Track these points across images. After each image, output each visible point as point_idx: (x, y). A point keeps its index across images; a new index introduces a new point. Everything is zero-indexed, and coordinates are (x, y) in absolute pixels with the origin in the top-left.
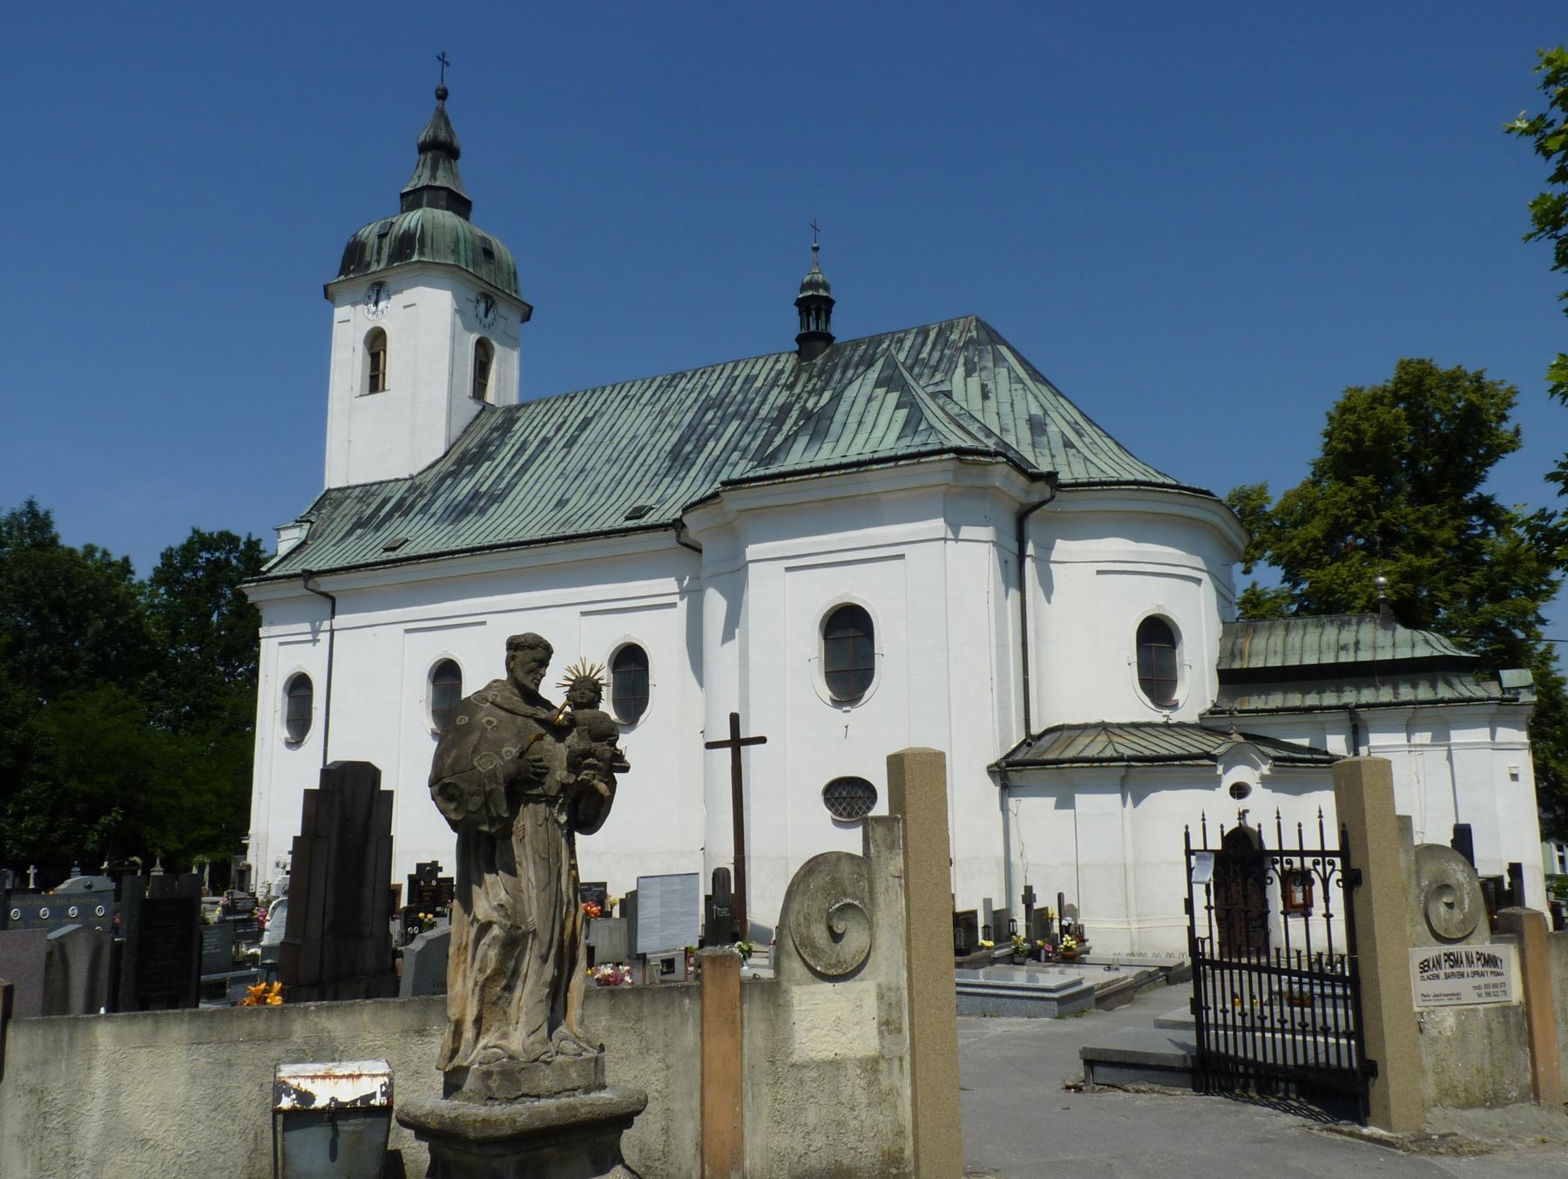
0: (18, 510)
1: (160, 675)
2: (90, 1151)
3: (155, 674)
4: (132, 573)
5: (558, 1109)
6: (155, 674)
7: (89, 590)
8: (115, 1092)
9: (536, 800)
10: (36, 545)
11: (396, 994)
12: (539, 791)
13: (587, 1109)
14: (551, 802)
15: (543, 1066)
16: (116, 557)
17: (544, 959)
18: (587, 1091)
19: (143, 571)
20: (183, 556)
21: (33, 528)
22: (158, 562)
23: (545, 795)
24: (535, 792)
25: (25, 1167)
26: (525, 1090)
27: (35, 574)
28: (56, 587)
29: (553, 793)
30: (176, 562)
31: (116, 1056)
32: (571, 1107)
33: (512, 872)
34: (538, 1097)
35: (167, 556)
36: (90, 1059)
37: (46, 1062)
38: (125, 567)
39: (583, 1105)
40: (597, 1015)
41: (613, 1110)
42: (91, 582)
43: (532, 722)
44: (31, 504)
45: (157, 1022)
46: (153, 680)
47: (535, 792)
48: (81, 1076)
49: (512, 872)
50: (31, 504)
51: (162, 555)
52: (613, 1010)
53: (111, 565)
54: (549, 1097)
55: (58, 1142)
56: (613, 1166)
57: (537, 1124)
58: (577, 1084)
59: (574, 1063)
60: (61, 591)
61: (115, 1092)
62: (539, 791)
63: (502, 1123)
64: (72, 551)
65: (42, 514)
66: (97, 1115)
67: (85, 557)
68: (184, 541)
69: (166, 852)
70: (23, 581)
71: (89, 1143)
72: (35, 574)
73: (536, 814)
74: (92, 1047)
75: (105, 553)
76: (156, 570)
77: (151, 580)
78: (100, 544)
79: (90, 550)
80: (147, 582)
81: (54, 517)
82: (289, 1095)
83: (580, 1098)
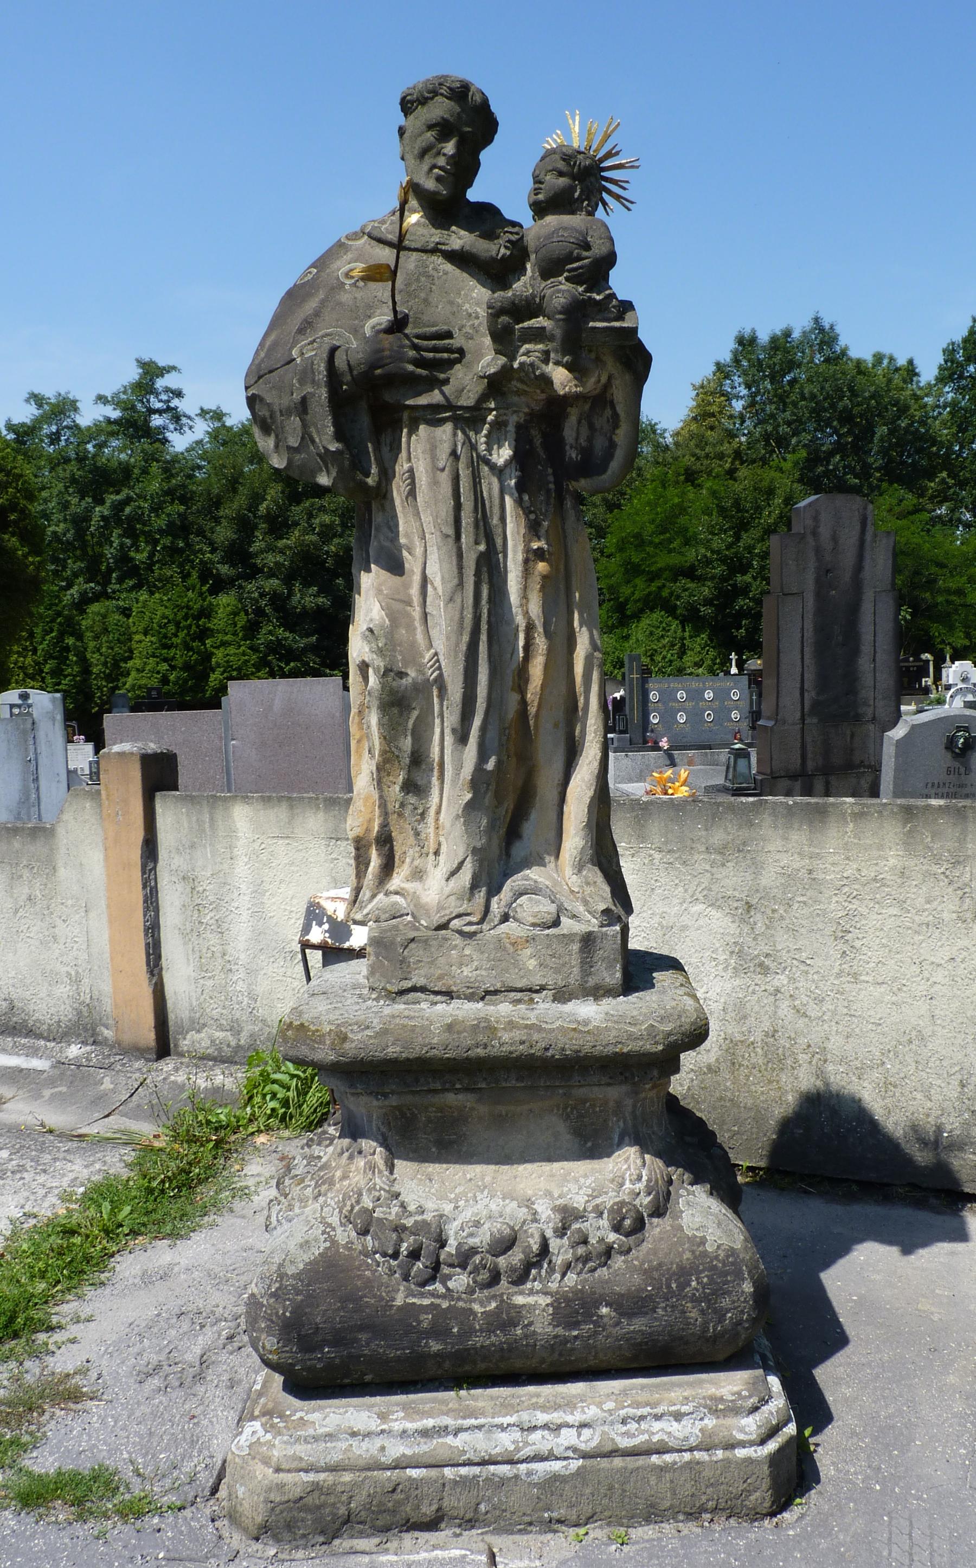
0: (808, 329)
1: (949, 476)
2: (242, 956)
3: (944, 474)
4: (917, 375)
5: (450, 1028)
6: (944, 474)
7: (872, 397)
8: (258, 891)
9: (432, 415)
10: (827, 360)
11: (874, 792)
12: (435, 397)
13: (518, 1035)
14: (468, 419)
15: (458, 940)
16: (901, 361)
17: (462, 739)
18: (562, 996)
19: (928, 372)
20: (965, 349)
21: (822, 343)
22: (940, 359)
23: (449, 406)
24: (423, 400)
25: (189, 964)
26: (421, 982)
27: (823, 388)
28: (841, 398)
29: (468, 400)
30: (960, 356)
31: (256, 845)
32: (487, 1027)
33: (396, 566)
34: (449, 995)
35: (949, 352)
36: (231, 847)
37: (193, 846)
38: (911, 371)
39: (511, 1025)
40: (880, 847)
41: (586, 1045)
42: (873, 389)
43: (438, 260)
44: (817, 320)
45: (291, 807)
46: (943, 481)
47: (423, 400)
48: (225, 866)
49: (396, 566)
50: (817, 320)
51: (944, 351)
52: (909, 842)
53: (897, 370)
54: (470, 998)
55: (213, 939)
56: (620, 1145)
57: (393, 1051)
58: (537, 980)
59: (530, 940)
60: (846, 401)
61: (258, 891)
62: (435, 397)
63: (321, 1039)
64: (859, 363)
65: (827, 327)
66: (245, 916)
67: (874, 366)
68: (965, 333)
69: (953, 648)
70: (813, 397)
71: (241, 946)
72: (823, 388)
73: (432, 451)
74: (232, 833)
75: (892, 359)
76: (941, 368)
77: (937, 379)
78: (886, 350)
79: (879, 358)
80: (933, 382)
81: (838, 329)
82: (320, 924)
83: (545, 1010)
